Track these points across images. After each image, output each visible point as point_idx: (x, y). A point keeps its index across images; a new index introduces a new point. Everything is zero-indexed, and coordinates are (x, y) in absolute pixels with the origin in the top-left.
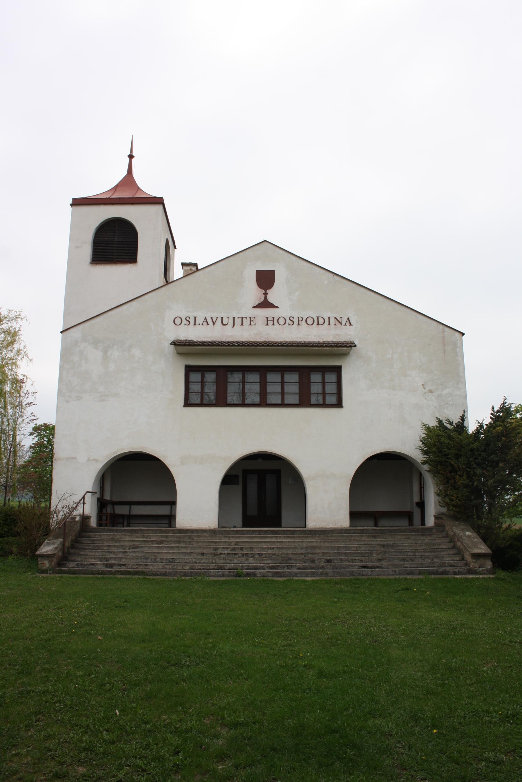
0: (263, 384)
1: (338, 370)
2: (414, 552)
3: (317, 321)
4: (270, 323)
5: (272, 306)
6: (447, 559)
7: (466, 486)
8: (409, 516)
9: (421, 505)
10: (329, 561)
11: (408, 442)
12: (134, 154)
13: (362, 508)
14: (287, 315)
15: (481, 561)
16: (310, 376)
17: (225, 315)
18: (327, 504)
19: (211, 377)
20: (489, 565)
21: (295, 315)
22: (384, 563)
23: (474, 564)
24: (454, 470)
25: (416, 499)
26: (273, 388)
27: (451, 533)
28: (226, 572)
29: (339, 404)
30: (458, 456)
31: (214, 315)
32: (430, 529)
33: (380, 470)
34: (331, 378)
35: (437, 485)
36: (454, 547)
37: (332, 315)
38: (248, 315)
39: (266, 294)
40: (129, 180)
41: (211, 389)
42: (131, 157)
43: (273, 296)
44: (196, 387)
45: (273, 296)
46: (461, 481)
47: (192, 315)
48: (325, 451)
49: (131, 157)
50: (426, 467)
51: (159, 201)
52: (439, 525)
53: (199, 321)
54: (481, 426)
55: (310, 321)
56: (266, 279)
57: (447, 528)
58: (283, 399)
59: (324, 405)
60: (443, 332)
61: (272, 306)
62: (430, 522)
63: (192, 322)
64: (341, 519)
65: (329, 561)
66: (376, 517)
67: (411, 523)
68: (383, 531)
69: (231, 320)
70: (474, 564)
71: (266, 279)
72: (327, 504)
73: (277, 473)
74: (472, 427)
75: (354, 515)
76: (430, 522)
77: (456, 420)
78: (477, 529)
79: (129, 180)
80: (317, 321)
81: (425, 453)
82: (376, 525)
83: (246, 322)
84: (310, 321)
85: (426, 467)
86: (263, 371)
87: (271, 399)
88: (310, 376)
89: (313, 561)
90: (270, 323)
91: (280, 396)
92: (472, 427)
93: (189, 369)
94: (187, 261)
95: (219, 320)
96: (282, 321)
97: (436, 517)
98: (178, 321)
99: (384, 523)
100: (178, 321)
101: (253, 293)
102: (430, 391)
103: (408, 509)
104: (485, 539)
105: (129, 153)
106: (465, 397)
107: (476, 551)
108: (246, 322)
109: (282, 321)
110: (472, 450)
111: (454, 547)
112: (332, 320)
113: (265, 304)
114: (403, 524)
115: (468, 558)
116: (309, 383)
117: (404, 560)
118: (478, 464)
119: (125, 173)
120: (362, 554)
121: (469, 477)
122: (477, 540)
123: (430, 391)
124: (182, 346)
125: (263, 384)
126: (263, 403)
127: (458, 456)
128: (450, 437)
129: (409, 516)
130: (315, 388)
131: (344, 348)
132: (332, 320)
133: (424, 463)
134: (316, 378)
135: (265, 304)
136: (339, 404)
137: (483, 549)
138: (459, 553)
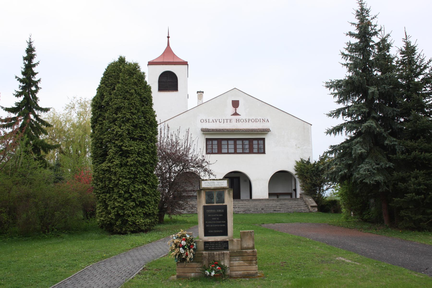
0: (235, 145)
1: (264, 139)
2: (292, 206)
3: (256, 121)
4: (238, 121)
5: (238, 115)
6: (303, 208)
7: (310, 183)
8: (291, 194)
9: (295, 190)
10: (262, 209)
11: (290, 167)
12: (170, 36)
13: (272, 192)
14: (244, 118)
15: (314, 208)
16: (253, 142)
17: (220, 118)
18: (260, 190)
19: (215, 142)
20: (316, 209)
21: (247, 118)
22: (281, 210)
23: (311, 209)
24: (306, 178)
25: (294, 188)
26: (239, 146)
27: (305, 200)
28: (218, 219)
29: (264, 153)
30: (307, 173)
31: (216, 119)
32: (298, 198)
33: (280, 177)
34: (261, 142)
35: (300, 182)
36: (306, 204)
37: (261, 118)
38: (229, 119)
39: (236, 110)
40: (168, 50)
41: (215, 147)
42: (168, 37)
43: (239, 111)
44: (210, 147)
45: (239, 111)
46: (308, 181)
47: (207, 118)
48: (259, 170)
49: (168, 37)
50: (297, 176)
51: (186, 63)
52: (301, 198)
53: (211, 121)
54: (316, 162)
55: (253, 121)
56: (236, 104)
57: (304, 198)
58: (243, 151)
59: (258, 153)
60: (304, 124)
61: (238, 115)
62: (298, 196)
63: (208, 121)
64: (266, 196)
65: (262, 209)
66: (277, 195)
67: (291, 197)
68: (281, 199)
69: (223, 120)
70: (311, 209)
71: (236, 104)
72: (260, 190)
73: (238, 178)
74: (312, 162)
75: (270, 194)
76: (298, 196)
77: (307, 160)
78: (314, 198)
79: (168, 50)
80: (256, 121)
81: (296, 171)
82: (278, 197)
83: (229, 121)
84: (253, 121)
85: (297, 176)
86: (235, 140)
87: (238, 151)
88: (253, 142)
89: (257, 209)
90: (238, 121)
91: (241, 150)
92: (312, 162)
93: (207, 140)
94: (199, 91)
95: (218, 120)
96: (242, 121)
97: (300, 195)
98: (202, 121)
99: (281, 197)
100: (202, 121)
101: (231, 110)
102: (299, 147)
103: (290, 192)
104: (316, 202)
105: (167, 36)
106: (312, 149)
107: (312, 205)
108: (229, 121)
109: (242, 121)
110: (312, 171)
111: (306, 204)
112: (261, 120)
113: (236, 114)
114: (289, 197)
115: (310, 207)
116: (253, 144)
117: (288, 208)
118: (314, 176)
119: (166, 46)
120: (274, 207)
121: (311, 180)
122: (313, 201)
123: (299, 147)
124: (205, 131)
125: (235, 145)
126: (235, 152)
127: (307, 173)
128: (304, 166)
129: (291, 194)
130: (255, 146)
131: (266, 131)
132: (261, 120)
133: (296, 174)
134: (255, 142)
135: (236, 114)
136: (264, 153)
137: (315, 204)
138: (307, 206)
